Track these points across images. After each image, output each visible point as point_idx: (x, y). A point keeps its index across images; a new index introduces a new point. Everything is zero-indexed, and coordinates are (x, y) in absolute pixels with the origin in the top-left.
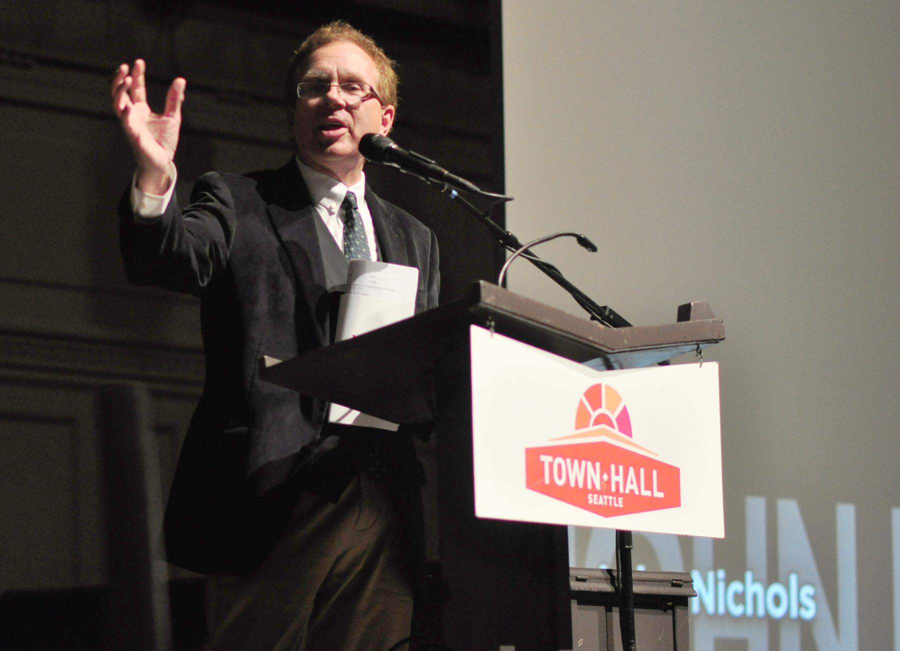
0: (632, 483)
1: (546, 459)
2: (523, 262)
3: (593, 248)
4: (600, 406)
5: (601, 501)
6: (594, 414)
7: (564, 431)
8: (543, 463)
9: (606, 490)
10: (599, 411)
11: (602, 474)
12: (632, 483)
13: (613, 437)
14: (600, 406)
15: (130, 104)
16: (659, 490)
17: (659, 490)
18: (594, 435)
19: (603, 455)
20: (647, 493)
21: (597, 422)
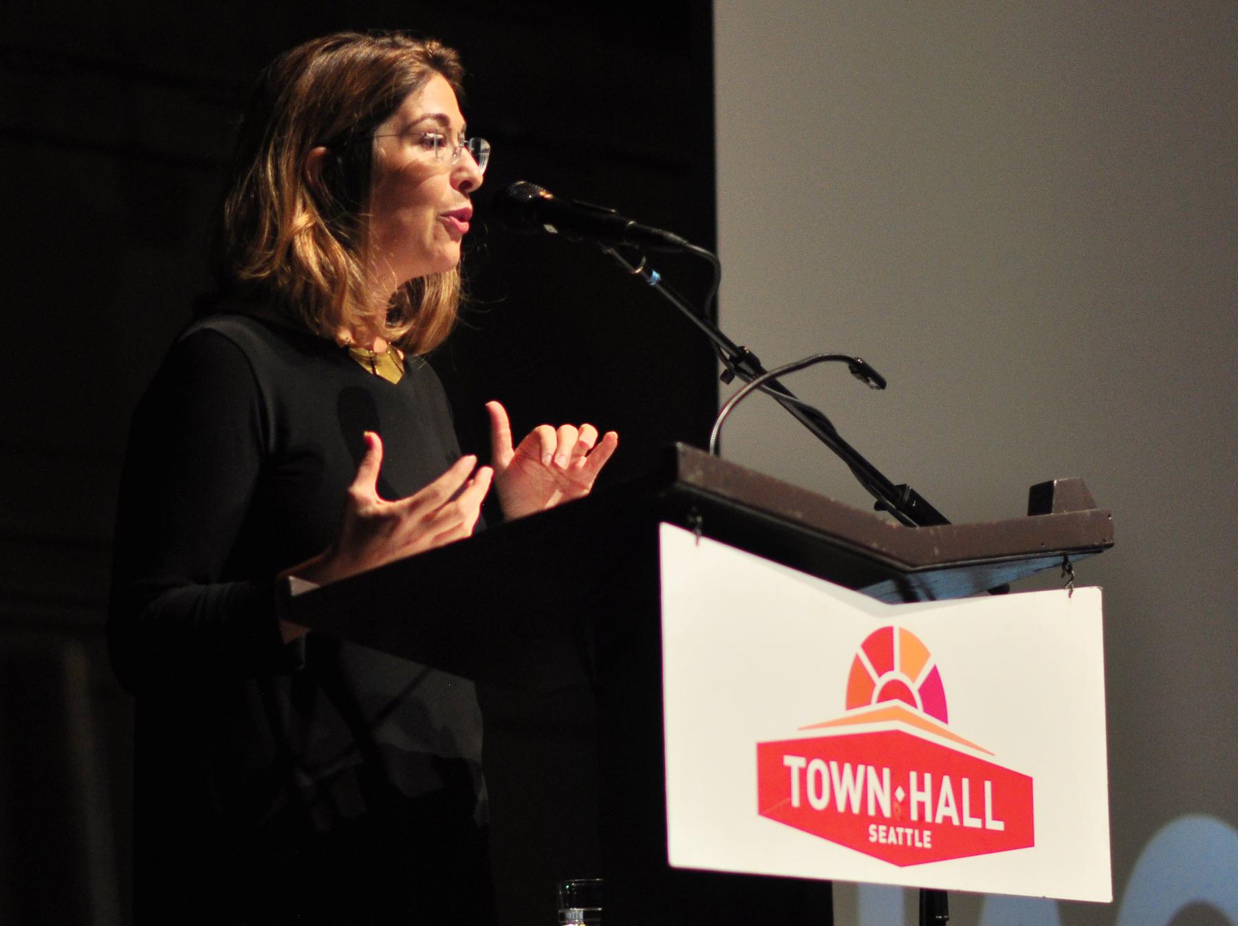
0: (947, 805)
1: (794, 762)
5: (893, 837)
6: (880, 682)
8: (789, 769)
9: (901, 817)
10: (889, 676)
12: (947, 805)
16: (995, 818)
17: (995, 818)
19: (896, 755)
20: (976, 823)
21: (885, 695)
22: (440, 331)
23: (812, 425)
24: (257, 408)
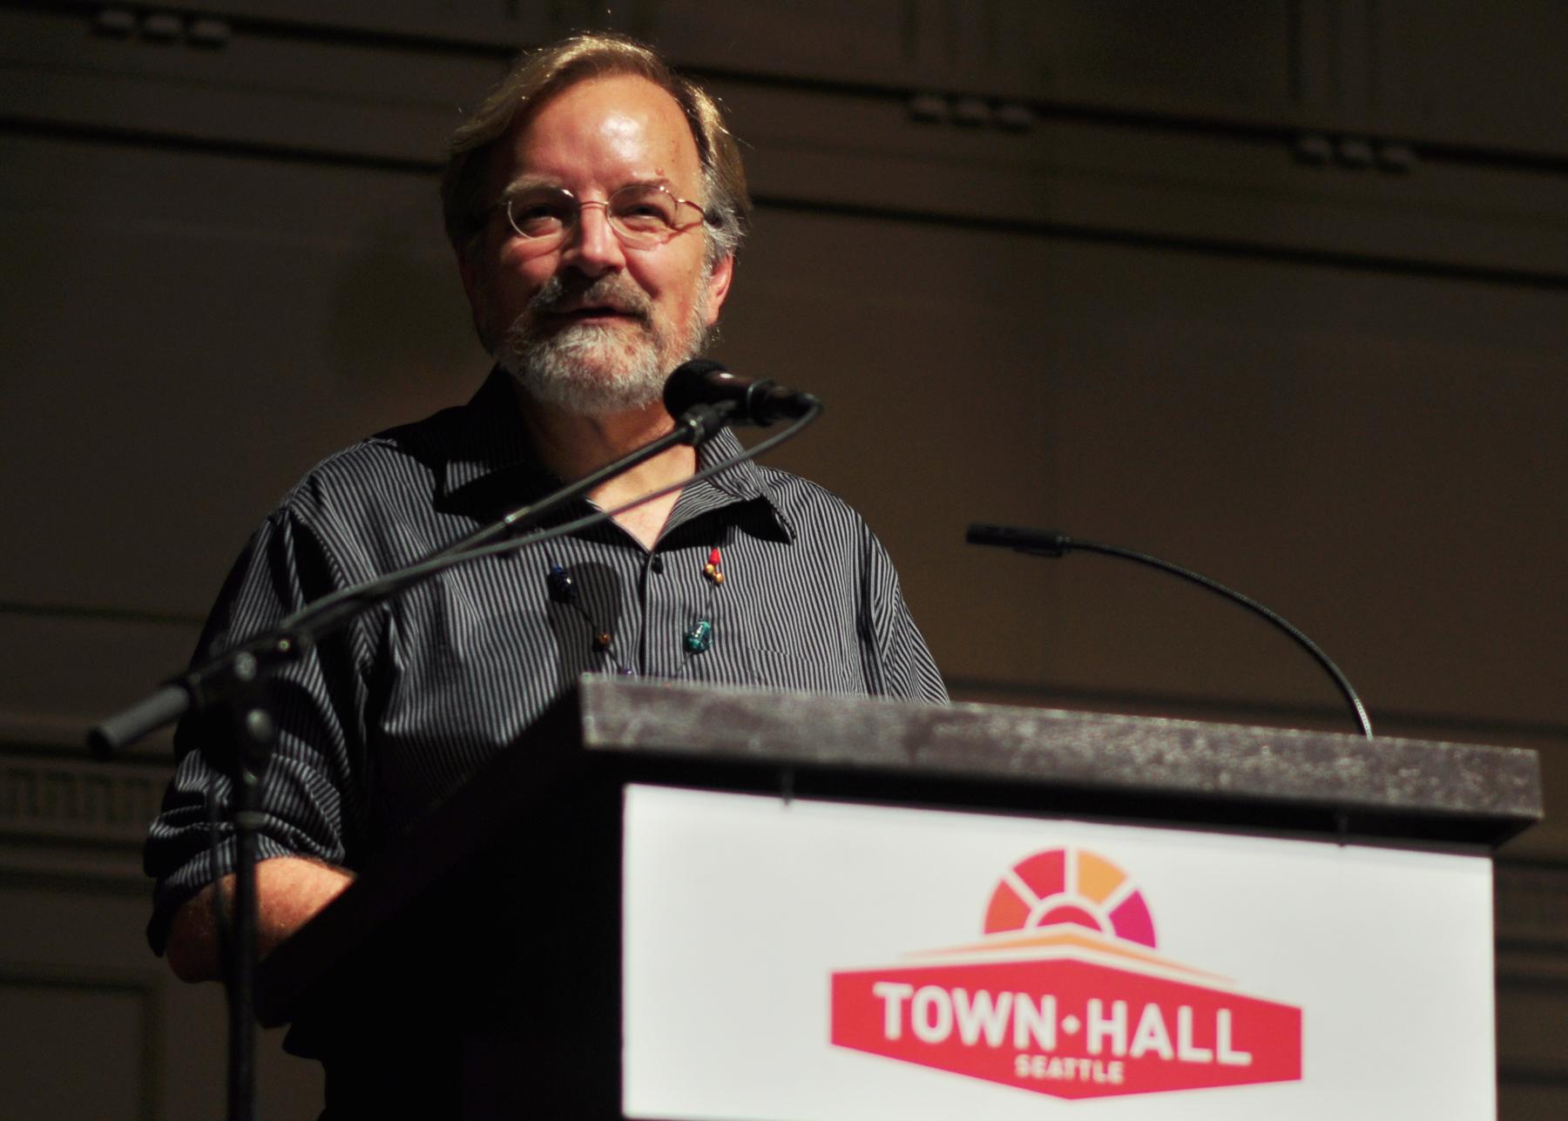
0: (1152, 1034)
1: (892, 994)
2: (633, 514)
3: (978, 536)
4: (1059, 887)
5: (1060, 1069)
6: (1040, 907)
7: (963, 938)
8: (881, 1003)
9: (1071, 1046)
10: (1054, 901)
11: (1060, 1016)
12: (1152, 1034)
13: (1107, 950)
14: (1059, 887)
15: (626, 683)
16: (1236, 1046)
17: (1236, 1046)
18: (1032, 944)
19: (1071, 985)
20: (1203, 1056)
21: (1052, 918)
22: (785, 428)
23: (1350, 763)
24: (630, 458)
